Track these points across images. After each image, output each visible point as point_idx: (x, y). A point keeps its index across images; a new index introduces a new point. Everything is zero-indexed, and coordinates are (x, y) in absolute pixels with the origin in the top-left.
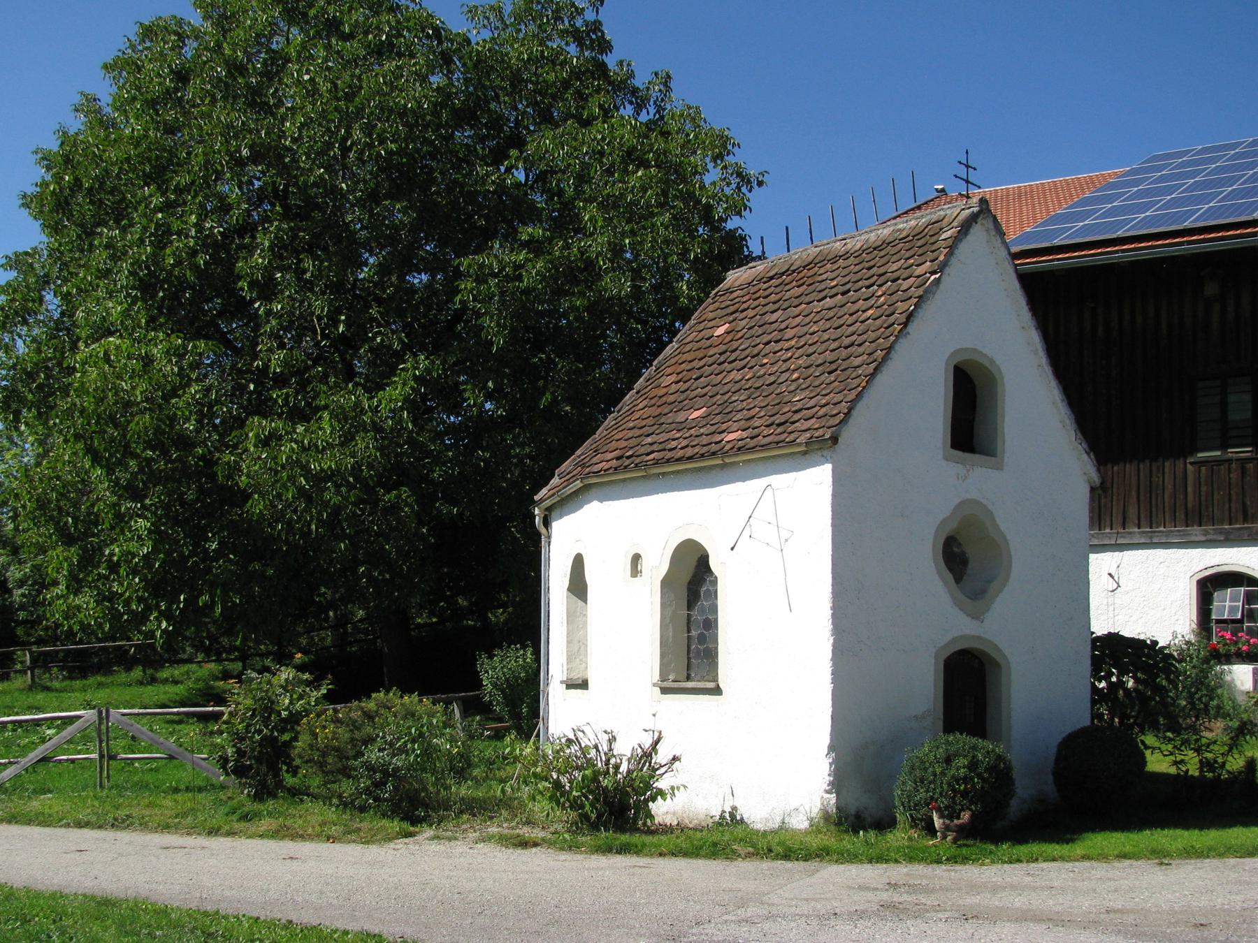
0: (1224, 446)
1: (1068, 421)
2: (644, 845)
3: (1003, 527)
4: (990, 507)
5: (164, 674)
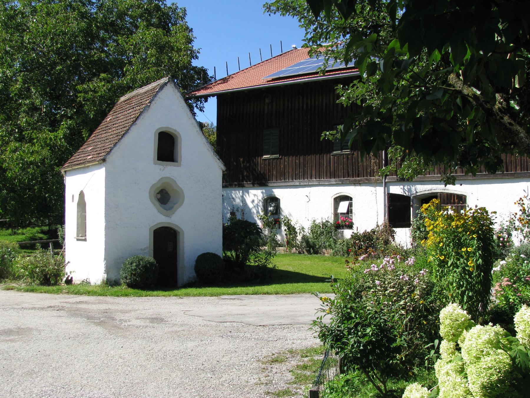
0: (341, 150)
1: (210, 149)
2: (54, 290)
3: (180, 186)
4: (175, 179)
5: (20, 231)
